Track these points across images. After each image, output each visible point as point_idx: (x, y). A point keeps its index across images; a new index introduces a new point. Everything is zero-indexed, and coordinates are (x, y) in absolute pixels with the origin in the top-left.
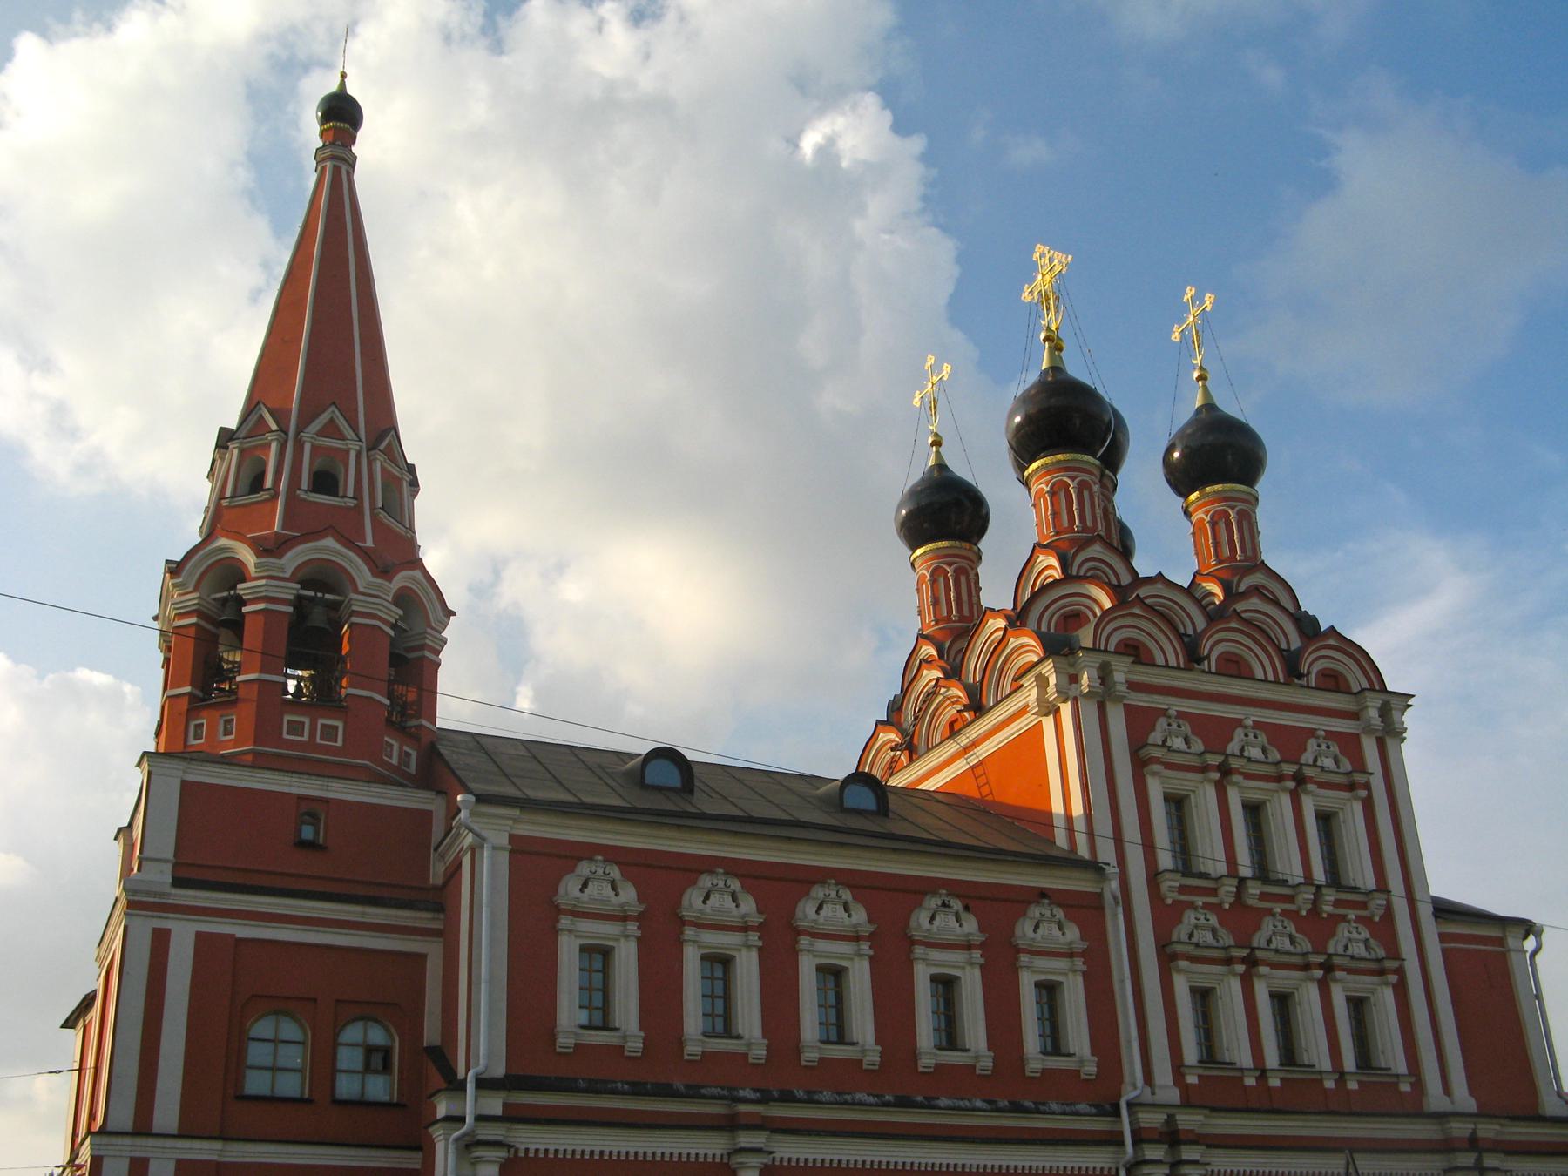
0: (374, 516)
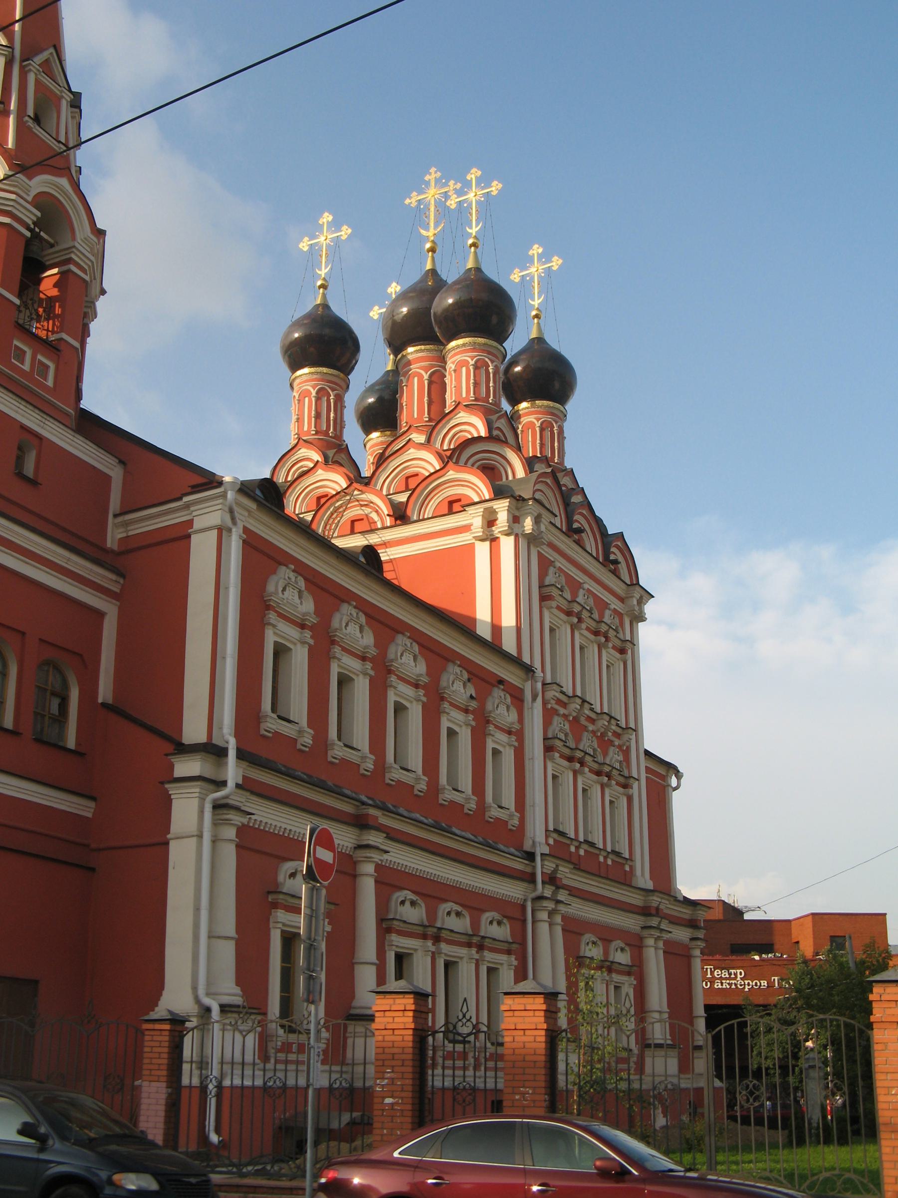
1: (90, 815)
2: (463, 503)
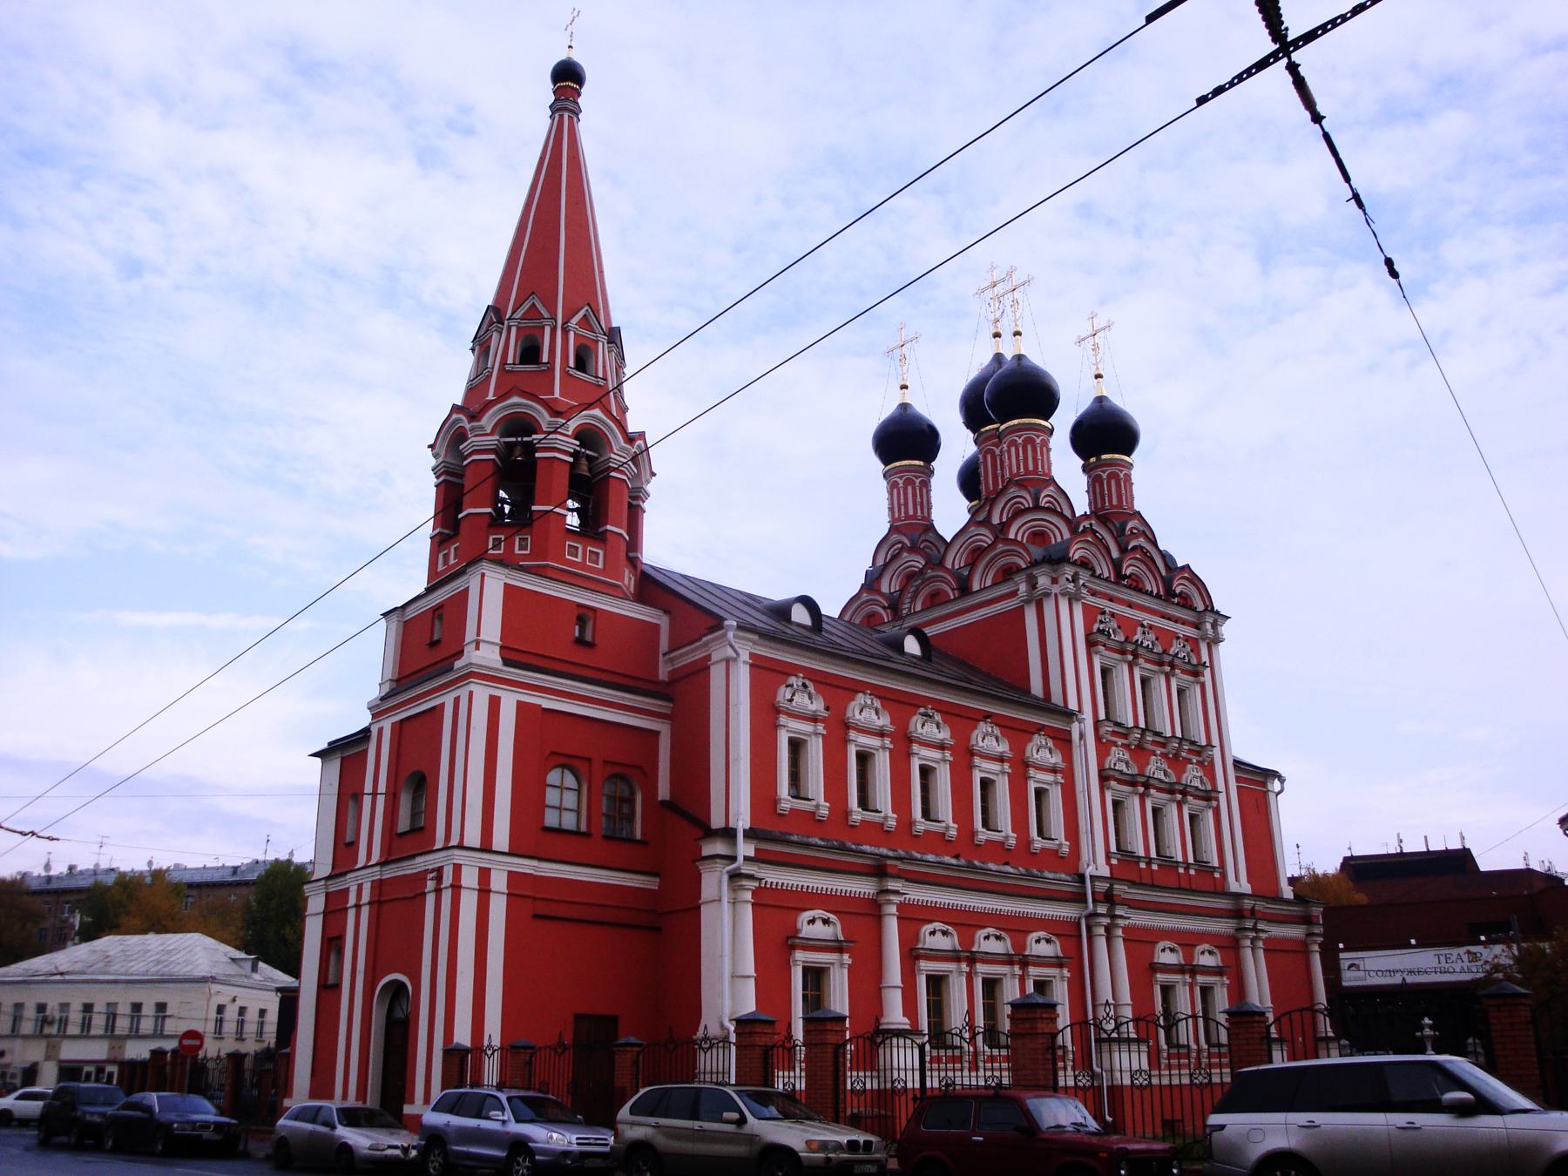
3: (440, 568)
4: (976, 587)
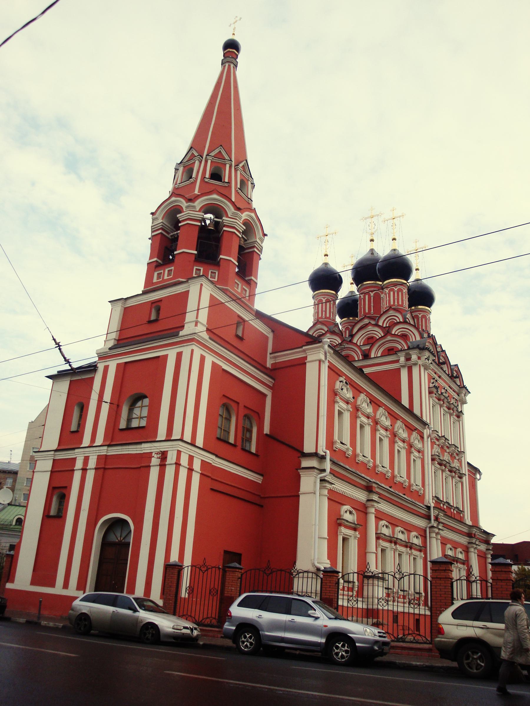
0: (236, 191)
1: (260, 482)
2: (395, 350)
3: (155, 280)
4: (372, 355)
